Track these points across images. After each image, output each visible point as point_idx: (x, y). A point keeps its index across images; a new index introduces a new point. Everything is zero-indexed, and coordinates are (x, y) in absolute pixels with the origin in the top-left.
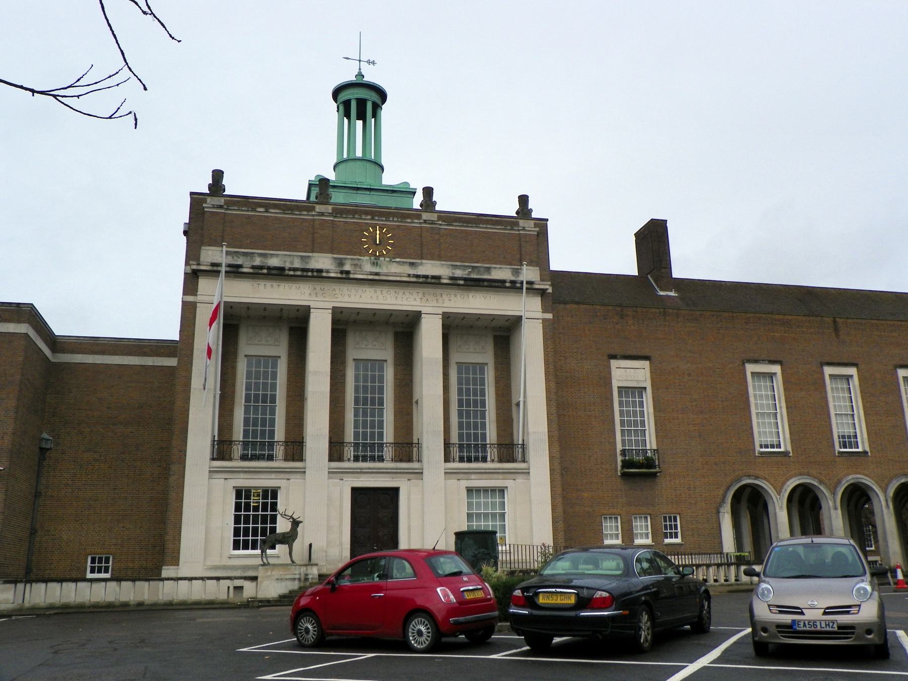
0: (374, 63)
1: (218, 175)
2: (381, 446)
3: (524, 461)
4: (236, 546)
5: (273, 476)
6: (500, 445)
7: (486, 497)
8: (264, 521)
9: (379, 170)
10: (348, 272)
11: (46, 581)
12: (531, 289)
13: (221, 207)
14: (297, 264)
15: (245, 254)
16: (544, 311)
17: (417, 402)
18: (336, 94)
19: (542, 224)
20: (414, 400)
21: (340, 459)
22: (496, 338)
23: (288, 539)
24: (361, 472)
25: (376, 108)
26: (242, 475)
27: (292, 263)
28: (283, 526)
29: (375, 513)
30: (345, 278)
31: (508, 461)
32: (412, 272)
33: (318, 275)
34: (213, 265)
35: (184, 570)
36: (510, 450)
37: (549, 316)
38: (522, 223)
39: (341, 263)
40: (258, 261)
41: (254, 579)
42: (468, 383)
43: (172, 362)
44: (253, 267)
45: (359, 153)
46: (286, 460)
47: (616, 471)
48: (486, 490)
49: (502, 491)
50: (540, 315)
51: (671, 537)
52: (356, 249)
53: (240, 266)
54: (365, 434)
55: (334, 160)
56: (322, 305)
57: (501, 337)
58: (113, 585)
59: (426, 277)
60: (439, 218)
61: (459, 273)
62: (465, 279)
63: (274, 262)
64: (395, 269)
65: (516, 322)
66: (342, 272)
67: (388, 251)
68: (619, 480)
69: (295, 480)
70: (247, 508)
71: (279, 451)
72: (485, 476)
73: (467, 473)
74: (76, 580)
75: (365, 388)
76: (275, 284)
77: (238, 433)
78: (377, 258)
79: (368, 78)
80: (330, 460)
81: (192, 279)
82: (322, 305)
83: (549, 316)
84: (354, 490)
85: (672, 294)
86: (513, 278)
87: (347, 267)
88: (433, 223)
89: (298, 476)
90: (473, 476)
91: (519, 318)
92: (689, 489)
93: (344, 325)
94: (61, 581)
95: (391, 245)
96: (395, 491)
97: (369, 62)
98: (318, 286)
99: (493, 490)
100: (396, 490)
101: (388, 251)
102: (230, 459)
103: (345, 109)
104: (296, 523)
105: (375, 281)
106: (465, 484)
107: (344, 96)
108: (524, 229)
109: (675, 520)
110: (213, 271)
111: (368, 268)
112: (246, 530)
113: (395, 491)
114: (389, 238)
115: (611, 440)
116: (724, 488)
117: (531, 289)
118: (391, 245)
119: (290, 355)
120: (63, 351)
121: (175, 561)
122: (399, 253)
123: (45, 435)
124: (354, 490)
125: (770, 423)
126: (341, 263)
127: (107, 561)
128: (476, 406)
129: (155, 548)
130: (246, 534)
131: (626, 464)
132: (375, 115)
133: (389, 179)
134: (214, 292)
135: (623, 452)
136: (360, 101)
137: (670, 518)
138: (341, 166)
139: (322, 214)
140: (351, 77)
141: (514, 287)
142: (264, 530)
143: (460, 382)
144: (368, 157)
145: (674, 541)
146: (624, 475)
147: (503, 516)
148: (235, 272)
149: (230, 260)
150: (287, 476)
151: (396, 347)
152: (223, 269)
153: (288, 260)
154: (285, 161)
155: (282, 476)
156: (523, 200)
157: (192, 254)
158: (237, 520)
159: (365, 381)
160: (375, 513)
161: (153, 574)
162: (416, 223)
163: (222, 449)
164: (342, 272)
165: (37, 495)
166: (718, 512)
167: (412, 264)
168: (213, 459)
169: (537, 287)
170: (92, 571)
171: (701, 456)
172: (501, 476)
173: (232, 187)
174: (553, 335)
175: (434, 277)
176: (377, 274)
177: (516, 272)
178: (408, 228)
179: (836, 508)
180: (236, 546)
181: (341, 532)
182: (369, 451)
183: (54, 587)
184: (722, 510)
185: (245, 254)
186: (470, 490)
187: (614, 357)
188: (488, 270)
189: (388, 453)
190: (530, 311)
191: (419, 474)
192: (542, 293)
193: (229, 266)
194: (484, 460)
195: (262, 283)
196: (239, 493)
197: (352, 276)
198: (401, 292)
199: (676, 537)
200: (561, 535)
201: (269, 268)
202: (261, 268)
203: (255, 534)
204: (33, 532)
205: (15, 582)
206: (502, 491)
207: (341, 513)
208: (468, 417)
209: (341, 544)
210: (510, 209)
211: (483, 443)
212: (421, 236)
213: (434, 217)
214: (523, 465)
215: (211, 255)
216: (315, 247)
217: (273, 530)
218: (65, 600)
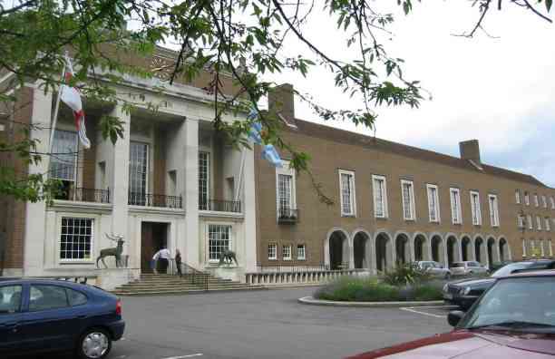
3: (240, 212)
4: (62, 256)
17: (103, 165)
41: (96, 277)
65: (178, 122)
68: (277, 226)
85: (294, 126)
91: (185, 118)
112: (69, 246)
121: (20, 264)
124: (143, 223)
125: (349, 204)
158: (63, 238)
180: (62, 256)
191: (183, 215)
194: (144, 204)
196: (64, 220)
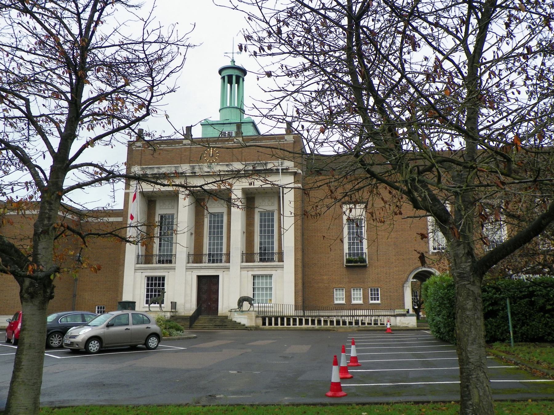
2: (221, 255)
5: (162, 271)
7: (262, 279)
17: (244, 232)
18: (220, 72)
20: (193, 235)
26: (149, 271)
29: (208, 288)
31: (251, 262)
39: (193, 168)
42: (265, 222)
43: (120, 219)
45: (228, 105)
47: (343, 264)
48: (262, 276)
49: (271, 276)
51: (375, 300)
52: (200, 160)
54: (214, 249)
55: (219, 108)
63: (163, 170)
66: (192, 173)
67: (216, 160)
68: (345, 270)
71: (276, 257)
72: (261, 269)
73: (252, 268)
77: (257, 250)
79: (237, 64)
84: (200, 278)
89: (173, 270)
90: (255, 269)
92: (386, 274)
95: (218, 156)
99: (266, 276)
100: (218, 276)
101: (216, 160)
102: (152, 263)
106: (251, 273)
107: (225, 73)
108: (286, 141)
109: (378, 291)
111: (206, 169)
114: (217, 153)
115: (341, 248)
116: (408, 273)
118: (218, 156)
122: (222, 160)
124: (200, 278)
126: (193, 168)
132: (238, 82)
137: (375, 289)
138: (221, 111)
139: (185, 145)
140: (229, 64)
144: (233, 105)
145: (376, 302)
147: (271, 289)
150: (168, 271)
153: (169, 169)
155: (166, 271)
158: (148, 291)
159: (214, 223)
160: (208, 288)
166: (403, 287)
167: (227, 165)
168: (138, 263)
169: (290, 171)
171: (395, 255)
172: (269, 269)
174: (304, 193)
184: (405, 285)
185: (150, 168)
186: (254, 277)
188: (266, 164)
192: (295, 174)
194: (221, 262)
197: (197, 174)
199: (378, 300)
206: (271, 276)
211: (263, 254)
214: (227, 264)
216: (182, 162)
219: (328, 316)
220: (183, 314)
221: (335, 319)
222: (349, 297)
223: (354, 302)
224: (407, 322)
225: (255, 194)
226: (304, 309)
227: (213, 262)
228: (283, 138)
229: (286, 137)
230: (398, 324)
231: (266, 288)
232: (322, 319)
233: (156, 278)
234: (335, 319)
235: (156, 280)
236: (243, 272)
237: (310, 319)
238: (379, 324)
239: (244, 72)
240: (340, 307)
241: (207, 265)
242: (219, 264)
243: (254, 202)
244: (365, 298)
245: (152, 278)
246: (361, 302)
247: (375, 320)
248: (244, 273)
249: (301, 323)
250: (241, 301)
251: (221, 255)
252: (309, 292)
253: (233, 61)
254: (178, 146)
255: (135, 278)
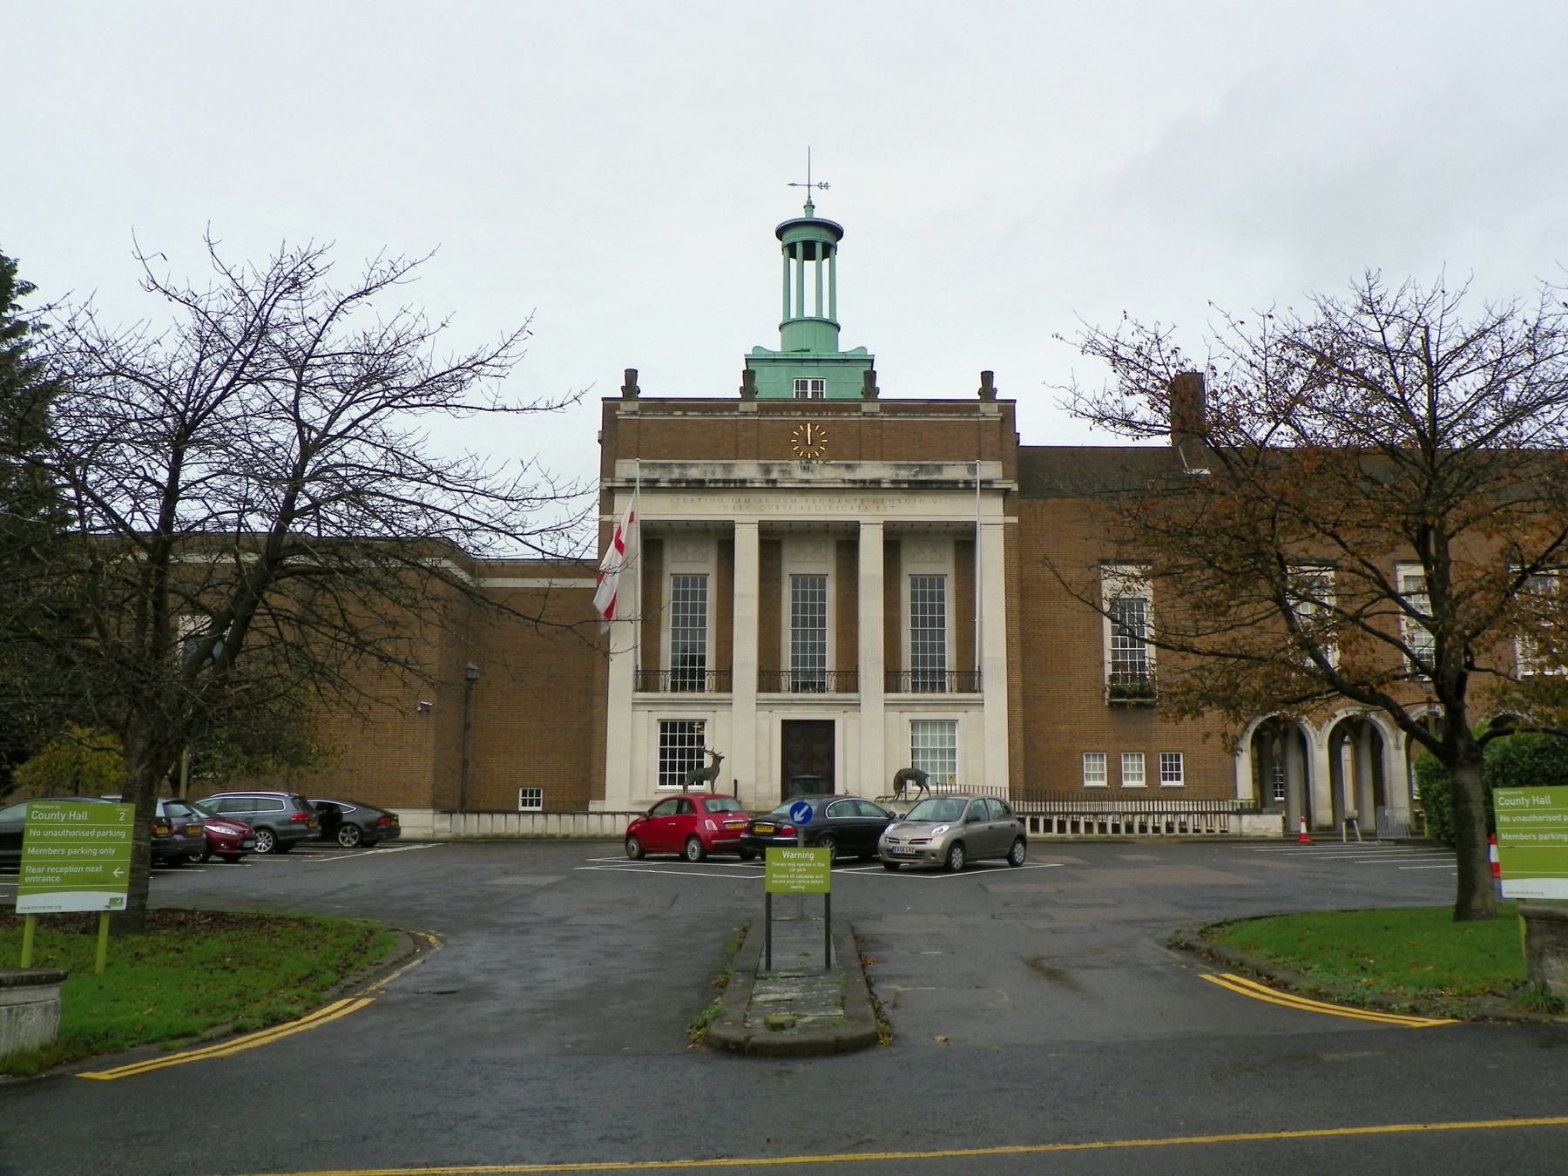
0: (827, 186)
1: (631, 375)
4: (663, 781)
6: (839, 673)
8: (691, 755)
9: (832, 330)
10: (774, 481)
11: (479, 812)
12: (987, 487)
13: (634, 413)
14: (719, 475)
15: (662, 466)
16: (1007, 513)
18: (781, 232)
19: (1009, 407)
21: (897, 690)
22: (957, 543)
23: (712, 774)
24: (792, 703)
25: (829, 250)
27: (713, 473)
28: (708, 761)
30: (772, 487)
32: (849, 476)
33: (741, 486)
34: (629, 481)
35: (609, 805)
36: (969, 679)
37: (1015, 520)
38: (983, 407)
40: (676, 474)
44: (671, 481)
46: (838, 691)
48: (934, 723)
49: (953, 723)
50: (1001, 520)
52: (785, 452)
53: (657, 481)
55: (780, 320)
56: (746, 519)
57: (964, 542)
58: (539, 818)
59: (863, 481)
60: (883, 409)
61: (904, 474)
62: (910, 482)
63: (694, 474)
64: (827, 473)
66: (768, 481)
69: (722, 712)
70: (673, 742)
71: (709, 681)
73: (912, 704)
74: (505, 813)
75: (804, 607)
76: (696, 498)
77: (666, 661)
78: (809, 461)
79: (818, 214)
80: (760, 690)
81: (607, 498)
82: (746, 519)
83: (1015, 520)
84: (784, 722)
86: (969, 477)
87: (774, 475)
88: (873, 415)
93: (773, 539)
94: (491, 812)
96: (829, 725)
97: (820, 186)
98: (743, 497)
102: (657, 690)
103: (791, 250)
104: (717, 759)
105: (806, 489)
106: (908, 716)
107: (791, 236)
110: (629, 487)
111: (799, 474)
112: (673, 765)
113: (829, 725)
117: (987, 487)
119: (719, 571)
120: (483, 575)
121: (601, 796)
123: (470, 665)
124: (784, 722)
126: (767, 470)
127: (538, 794)
128: (932, 625)
129: (584, 785)
130: (673, 768)
131: (1116, 693)
133: (847, 343)
134: (633, 510)
135: (1113, 678)
136: (811, 240)
138: (786, 328)
139: (746, 414)
140: (801, 214)
141: (968, 487)
142: (691, 765)
143: (914, 596)
146: (1111, 704)
147: (953, 752)
148: (651, 486)
149: (647, 474)
151: (838, 559)
152: (638, 485)
153: (710, 469)
154: (700, 365)
156: (987, 377)
157: (607, 470)
158: (663, 754)
161: (581, 809)
162: (854, 416)
163: (647, 679)
164: (768, 481)
165: (467, 727)
167: (848, 467)
170: (524, 804)
173: (649, 388)
174: (1018, 544)
175: (872, 482)
176: (808, 481)
177: (972, 469)
178: (844, 424)
179: (1398, 748)
180: (663, 781)
181: (771, 767)
182: (808, 683)
183: (486, 818)
185: (662, 466)
186: (914, 724)
187: (1105, 562)
188: (939, 468)
189: (831, 681)
190: (989, 519)
192: (1006, 493)
193: (646, 481)
194: (943, 690)
195: (681, 497)
196: (664, 725)
198: (843, 499)
199: (1178, 779)
200: (1020, 775)
201: (687, 481)
202: (679, 481)
203: (682, 768)
204: (465, 764)
205: (451, 812)
206: (953, 723)
207: (770, 748)
208: (923, 638)
209: (771, 780)
210: (969, 390)
212: (859, 432)
213: (875, 407)
215: (629, 468)
216: (739, 453)
217: (701, 764)
218: (496, 831)
219: (1095, 814)
220: (753, 808)
221: (1109, 821)
222: (1115, 774)
223: (1127, 783)
224: (1264, 827)
225: (782, 533)
226: (1029, 796)
227: (924, 690)
228: (977, 409)
229: (983, 407)
230: (1245, 831)
231: (942, 752)
232: (1082, 820)
233: (682, 724)
234: (1109, 821)
235: (682, 729)
236: (891, 714)
237: (1055, 819)
238: (1190, 832)
239: (838, 232)
240: (1096, 794)
241: (910, 695)
242: (697, 695)
243: (779, 550)
244: (1151, 774)
245: (673, 724)
246: (1142, 783)
247: (1167, 824)
248: (894, 715)
249: (1048, 827)
250: (900, 782)
251: (823, 672)
252: (1039, 761)
253: (810, 206)
254: (727, 416)
255: (633, 723)
